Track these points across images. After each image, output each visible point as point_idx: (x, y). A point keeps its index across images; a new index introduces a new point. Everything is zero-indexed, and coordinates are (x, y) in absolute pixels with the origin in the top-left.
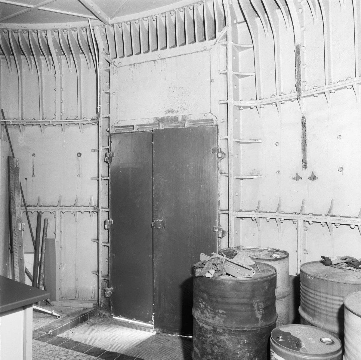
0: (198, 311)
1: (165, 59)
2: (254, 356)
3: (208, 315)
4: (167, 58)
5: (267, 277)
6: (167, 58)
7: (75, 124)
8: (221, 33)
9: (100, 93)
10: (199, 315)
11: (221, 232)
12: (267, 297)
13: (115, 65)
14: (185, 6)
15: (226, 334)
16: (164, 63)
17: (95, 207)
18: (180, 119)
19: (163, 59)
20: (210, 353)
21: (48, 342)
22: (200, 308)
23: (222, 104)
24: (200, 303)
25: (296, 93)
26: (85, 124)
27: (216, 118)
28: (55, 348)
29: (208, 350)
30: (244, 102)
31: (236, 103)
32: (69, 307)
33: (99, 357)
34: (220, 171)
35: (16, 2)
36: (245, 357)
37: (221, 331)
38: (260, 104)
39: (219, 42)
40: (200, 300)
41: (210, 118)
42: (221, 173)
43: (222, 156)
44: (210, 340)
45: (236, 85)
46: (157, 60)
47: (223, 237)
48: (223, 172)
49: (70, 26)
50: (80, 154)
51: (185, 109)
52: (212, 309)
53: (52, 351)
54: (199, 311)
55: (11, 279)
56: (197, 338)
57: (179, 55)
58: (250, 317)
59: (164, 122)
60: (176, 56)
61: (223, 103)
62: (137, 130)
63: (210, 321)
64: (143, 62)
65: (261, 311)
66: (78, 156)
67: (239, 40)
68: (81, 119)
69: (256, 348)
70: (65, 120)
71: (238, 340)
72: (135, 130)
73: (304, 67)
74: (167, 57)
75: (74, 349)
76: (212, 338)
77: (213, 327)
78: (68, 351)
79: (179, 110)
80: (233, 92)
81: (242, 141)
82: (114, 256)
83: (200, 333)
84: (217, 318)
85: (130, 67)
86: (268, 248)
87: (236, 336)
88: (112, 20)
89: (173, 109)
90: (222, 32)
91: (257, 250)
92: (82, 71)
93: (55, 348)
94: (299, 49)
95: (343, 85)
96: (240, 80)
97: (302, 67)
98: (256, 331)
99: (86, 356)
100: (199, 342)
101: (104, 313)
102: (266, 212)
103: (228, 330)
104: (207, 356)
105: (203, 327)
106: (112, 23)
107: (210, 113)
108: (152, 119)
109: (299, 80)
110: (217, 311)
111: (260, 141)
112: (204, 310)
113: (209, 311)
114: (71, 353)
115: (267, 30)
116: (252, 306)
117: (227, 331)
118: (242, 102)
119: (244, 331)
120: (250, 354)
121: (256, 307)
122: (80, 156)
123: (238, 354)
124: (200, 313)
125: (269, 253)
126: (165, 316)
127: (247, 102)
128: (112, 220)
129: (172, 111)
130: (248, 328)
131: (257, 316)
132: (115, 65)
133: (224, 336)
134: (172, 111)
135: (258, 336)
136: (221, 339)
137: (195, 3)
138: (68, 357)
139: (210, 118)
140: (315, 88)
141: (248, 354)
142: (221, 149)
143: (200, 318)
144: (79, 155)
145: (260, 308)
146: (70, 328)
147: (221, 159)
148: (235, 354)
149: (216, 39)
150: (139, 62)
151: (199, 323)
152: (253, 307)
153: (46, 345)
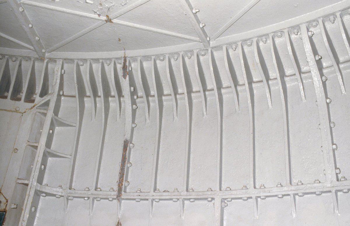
8: (42, 99)
25: (116, 193)
27: (5, 201)
38: (69, 195)
39: (37, 108)
45: (44, 162)
55: (18, 96)
67: (60, 113)
73: (129, 165)
80: (40, 172)
90: (43, 98)
94: (127, 145)
95: (170, 196)
96: (50, 159)
97: (127, 165)
109: (122, 178)
115: (95, 114)
118: (47, 187)
137: (20, 56)
140: (138, 191)
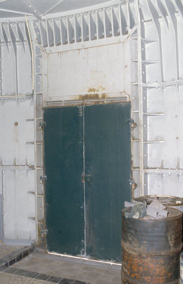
0: (127, 243)
1: (87, 48)
2: (168, 273)
3: (135, 245)
4: (89, 48)
5: (176, 217)
6: (89, 48)
7: (12, 99)
8: (132, 30)
9: (34, 75)
10: (128, 245)
11: (134, 184)
12: (176, 231)
13: (46, 52)
14: (104, 8)
15: (148, 258)
16: (87, 52)
17: (30, 166)
18: (100, 96)
19: (86, 48)
20: (136, 272)
21: (4, 271)
22: (129, 241)
23: (134, 85)
24: (129, 237)
26: (21, 99)
28: (12, 275)
29: (135, 270)
30: (150, 84)
31: (144, 85)
32: (12, 246)
33: (47, 281)
34: (133, 137)
35: (29, 35)
36: (162, 273)
37: (145, 256)
38: (163, 85)
40: (129, 235)
41: (125, 96)
42: (133, 139)
43: (134, 126)
44: (137, 262)
46: (81, 49)
47: (135, 188)
48: (135, 138)
49: (9, 20)
50: (17, 123)
51: (104, 89)
52: (138, 241)
53: (10, 278)
54: (128, 243)
56: (126, 262)
57: (99, 46)
58: (165, 245)
59: (87, 98)
60: (96, 47)
61: (135, 85)
62: (65, 104)
63: (137, 249)
64: (69, 51)
65: (173, 241)
66: (15, 125)
68: (17, 95)
69: (169, 267)
70: (4, 96)
71: (157, 262)
72: (64, 104)
74: (89, 47)
75: (26, 276)
76: (138, 261)
77: (139, 253)
78: (22, 278)
79: (99, 89)
81: (149, 114)
82: (47, 205)
83: (128, 258)
84: (142, 247)
85: (59, 54)
86: (170, 196)
87: (156, 259)
88: (44, 16)
89: (95, 88)
91: (163, 198)
92: (17, 56)
93: (12, 275)
98: (169, 255)
99: (36, 280)
100: (127, 264)
101: (40, 250)
102: (168, 169)
103: (150, 255)
104: (135, 274)
105: (131, 254)
106: (44, 19)
107: (124, 92)
108: (78, 96)
110: (142, 242)
111: (163, 114)
112: (132, 241)
113: (136, 242)
114: (24, 279)
116: (167, 238)
117: (149, 256)
119: (161, 255)
120: (165, 271)
121: (169, 238)
122: (17, 125)
123: (157, 271)
124: (129, 244)
125: (172, 200)
126: (94, 247)
127: (154, 84)
128: (46, 177)
129: (94, 90)
130: (164, 253)
131: (170, 245)
132: (46, 52)
133: (147, 259)
134: (94, 90)
135: (171, 258)
136: (145, 262)
138: (23, 281)
139: (124, 96)
141: (164, 271)
142: (133, 120)
143: (129, 247)
144: (16, 124)
145: (172, 239)
146: (17, 262)
147: (133, 128)
148: (155, 271)
149: (128, 34)
150: (66, 50)
151: (128, 251)
152: (168, 238)
153: (4, 274)
